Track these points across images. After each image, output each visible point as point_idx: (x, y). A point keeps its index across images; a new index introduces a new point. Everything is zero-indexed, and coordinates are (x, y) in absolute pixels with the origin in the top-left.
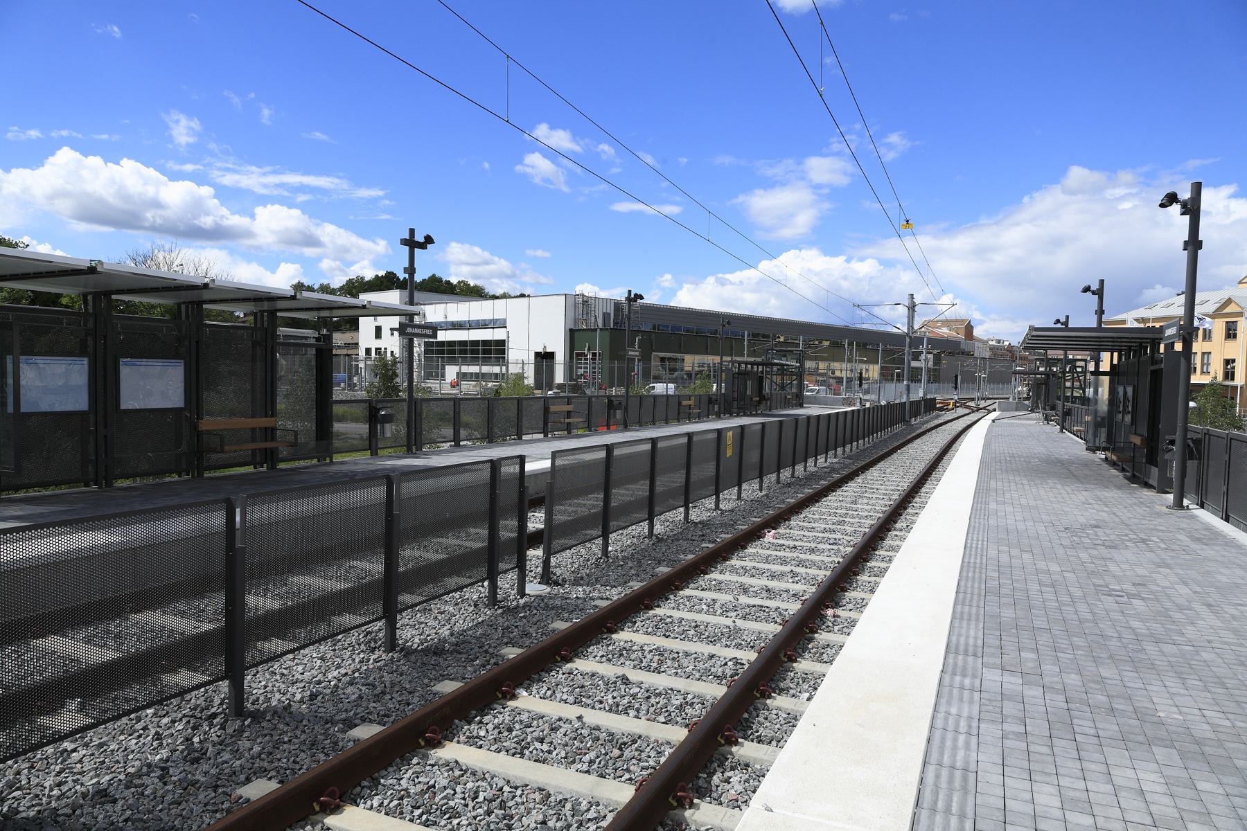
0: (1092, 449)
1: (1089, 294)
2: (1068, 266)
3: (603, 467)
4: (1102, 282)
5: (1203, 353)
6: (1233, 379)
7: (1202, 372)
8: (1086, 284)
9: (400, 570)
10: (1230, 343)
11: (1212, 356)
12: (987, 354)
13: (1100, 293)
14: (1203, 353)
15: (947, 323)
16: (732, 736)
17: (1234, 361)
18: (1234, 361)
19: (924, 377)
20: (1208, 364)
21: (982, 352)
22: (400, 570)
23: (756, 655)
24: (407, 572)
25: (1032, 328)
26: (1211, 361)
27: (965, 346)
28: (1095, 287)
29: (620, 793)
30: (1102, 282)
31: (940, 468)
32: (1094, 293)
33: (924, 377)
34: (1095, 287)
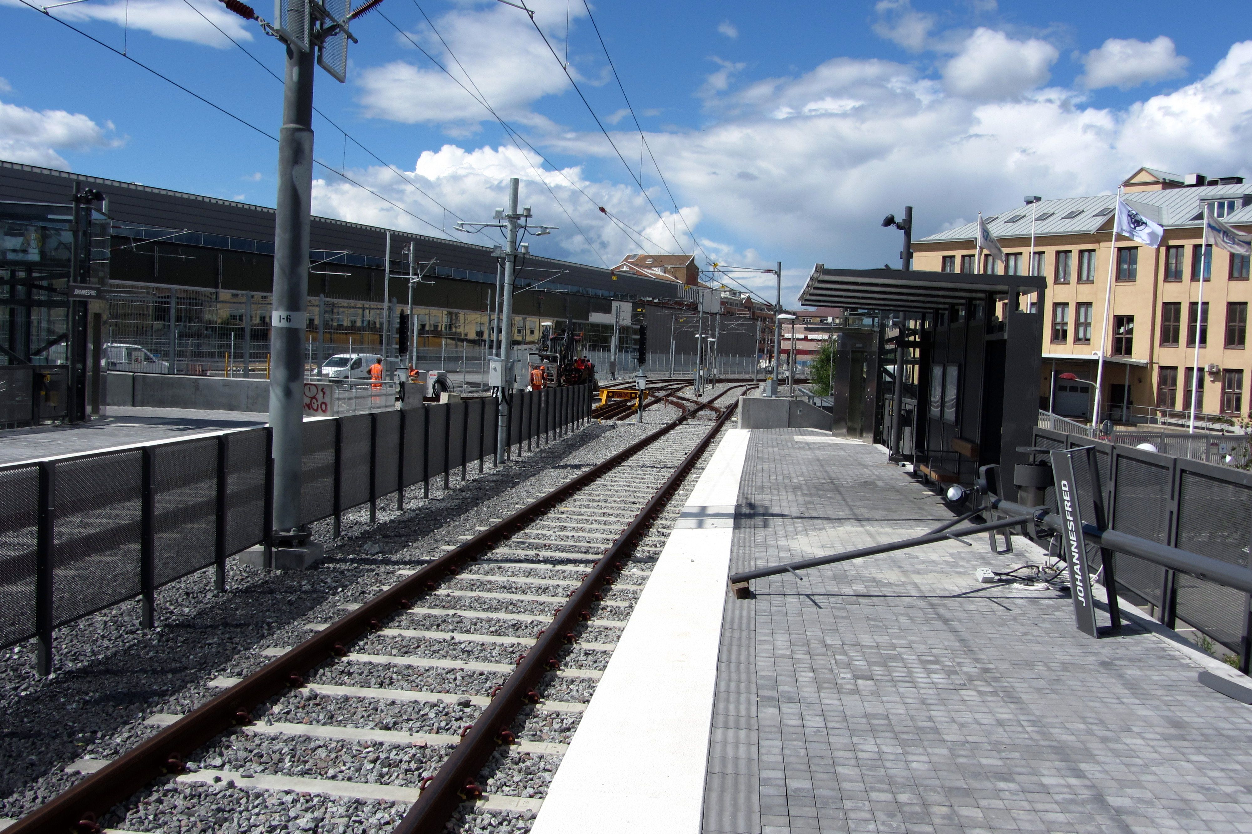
0: (896, 458)
1: (893, 227)
2: (855, 191)
3: (36, 483)
4: (910, 210)
5: (1079, 305)
6: (1129, 352)
7: (1077, 340)
8: (887, 214)
9: (56, 542)
10: (1125, 288)
11: (1094, 311)
12: (716, 308)
13: (906, 227)
14: (1079, 305)
15: (658, 260)
16: (474, 789)
17: (1130, 319)
18: (1130, 319)
19: (614, 341)
20: (1087, 325)
21: (710, 305)
22: (56, 542)
23: (514, 666)
24: (61, 545)
25: (820, 269)
26: (1092, 319)
27: (686, 294)
28: (900, 218)
29: (407, 796)
30: (910, 210)
31: (706, 455)
32: (899, 227)
33: (614, 341)
34: (900, 218)
